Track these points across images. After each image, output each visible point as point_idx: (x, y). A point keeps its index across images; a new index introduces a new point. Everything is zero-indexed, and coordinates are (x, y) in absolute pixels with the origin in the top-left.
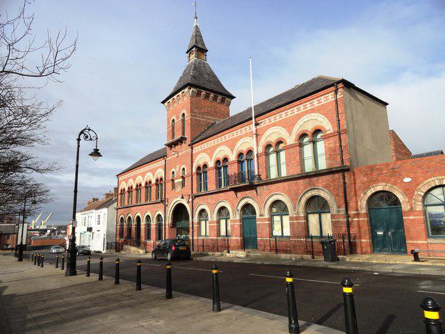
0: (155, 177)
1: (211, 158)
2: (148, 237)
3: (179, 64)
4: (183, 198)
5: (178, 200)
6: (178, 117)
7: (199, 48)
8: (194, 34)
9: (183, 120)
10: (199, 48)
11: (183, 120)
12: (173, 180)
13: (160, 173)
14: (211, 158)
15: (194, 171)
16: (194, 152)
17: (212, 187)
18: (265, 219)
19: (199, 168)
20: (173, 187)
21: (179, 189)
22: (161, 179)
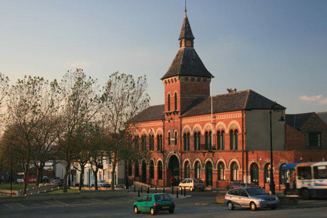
0: (229, 127)
1: (203, 128)
2: (152, 176)
3: (172, 50)
4: (175, 153)
5: (172, 153)
6: (172, 95)
7: (187, 36)
8: (184, 26)
9: (176, 97)
10: (187, 36)
11: (176, 97)
12: (169, 138)
13: (160, 130)
14: (203, 128)
15: (182, 135)
16: (182, 123)
17: (192, 148)
18: (216, 171)
19: (185, 134)
20: (169, 143)
21: (173, 145)
22: (161, 136)
